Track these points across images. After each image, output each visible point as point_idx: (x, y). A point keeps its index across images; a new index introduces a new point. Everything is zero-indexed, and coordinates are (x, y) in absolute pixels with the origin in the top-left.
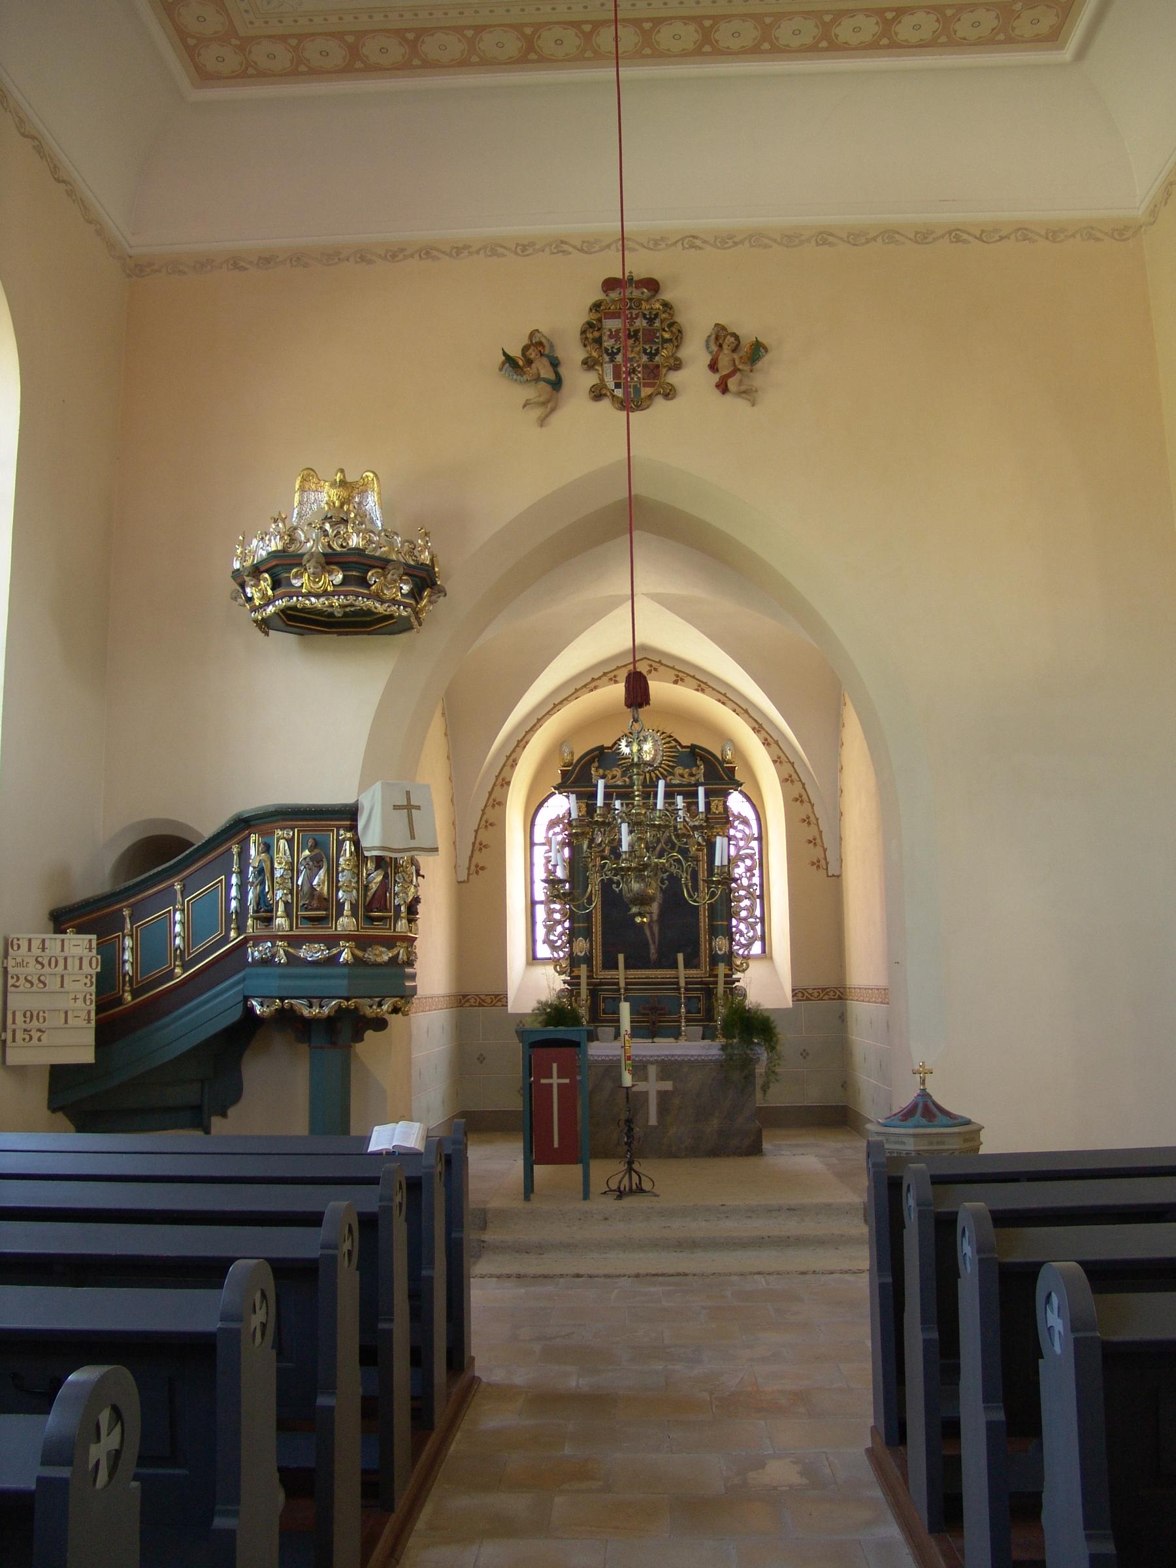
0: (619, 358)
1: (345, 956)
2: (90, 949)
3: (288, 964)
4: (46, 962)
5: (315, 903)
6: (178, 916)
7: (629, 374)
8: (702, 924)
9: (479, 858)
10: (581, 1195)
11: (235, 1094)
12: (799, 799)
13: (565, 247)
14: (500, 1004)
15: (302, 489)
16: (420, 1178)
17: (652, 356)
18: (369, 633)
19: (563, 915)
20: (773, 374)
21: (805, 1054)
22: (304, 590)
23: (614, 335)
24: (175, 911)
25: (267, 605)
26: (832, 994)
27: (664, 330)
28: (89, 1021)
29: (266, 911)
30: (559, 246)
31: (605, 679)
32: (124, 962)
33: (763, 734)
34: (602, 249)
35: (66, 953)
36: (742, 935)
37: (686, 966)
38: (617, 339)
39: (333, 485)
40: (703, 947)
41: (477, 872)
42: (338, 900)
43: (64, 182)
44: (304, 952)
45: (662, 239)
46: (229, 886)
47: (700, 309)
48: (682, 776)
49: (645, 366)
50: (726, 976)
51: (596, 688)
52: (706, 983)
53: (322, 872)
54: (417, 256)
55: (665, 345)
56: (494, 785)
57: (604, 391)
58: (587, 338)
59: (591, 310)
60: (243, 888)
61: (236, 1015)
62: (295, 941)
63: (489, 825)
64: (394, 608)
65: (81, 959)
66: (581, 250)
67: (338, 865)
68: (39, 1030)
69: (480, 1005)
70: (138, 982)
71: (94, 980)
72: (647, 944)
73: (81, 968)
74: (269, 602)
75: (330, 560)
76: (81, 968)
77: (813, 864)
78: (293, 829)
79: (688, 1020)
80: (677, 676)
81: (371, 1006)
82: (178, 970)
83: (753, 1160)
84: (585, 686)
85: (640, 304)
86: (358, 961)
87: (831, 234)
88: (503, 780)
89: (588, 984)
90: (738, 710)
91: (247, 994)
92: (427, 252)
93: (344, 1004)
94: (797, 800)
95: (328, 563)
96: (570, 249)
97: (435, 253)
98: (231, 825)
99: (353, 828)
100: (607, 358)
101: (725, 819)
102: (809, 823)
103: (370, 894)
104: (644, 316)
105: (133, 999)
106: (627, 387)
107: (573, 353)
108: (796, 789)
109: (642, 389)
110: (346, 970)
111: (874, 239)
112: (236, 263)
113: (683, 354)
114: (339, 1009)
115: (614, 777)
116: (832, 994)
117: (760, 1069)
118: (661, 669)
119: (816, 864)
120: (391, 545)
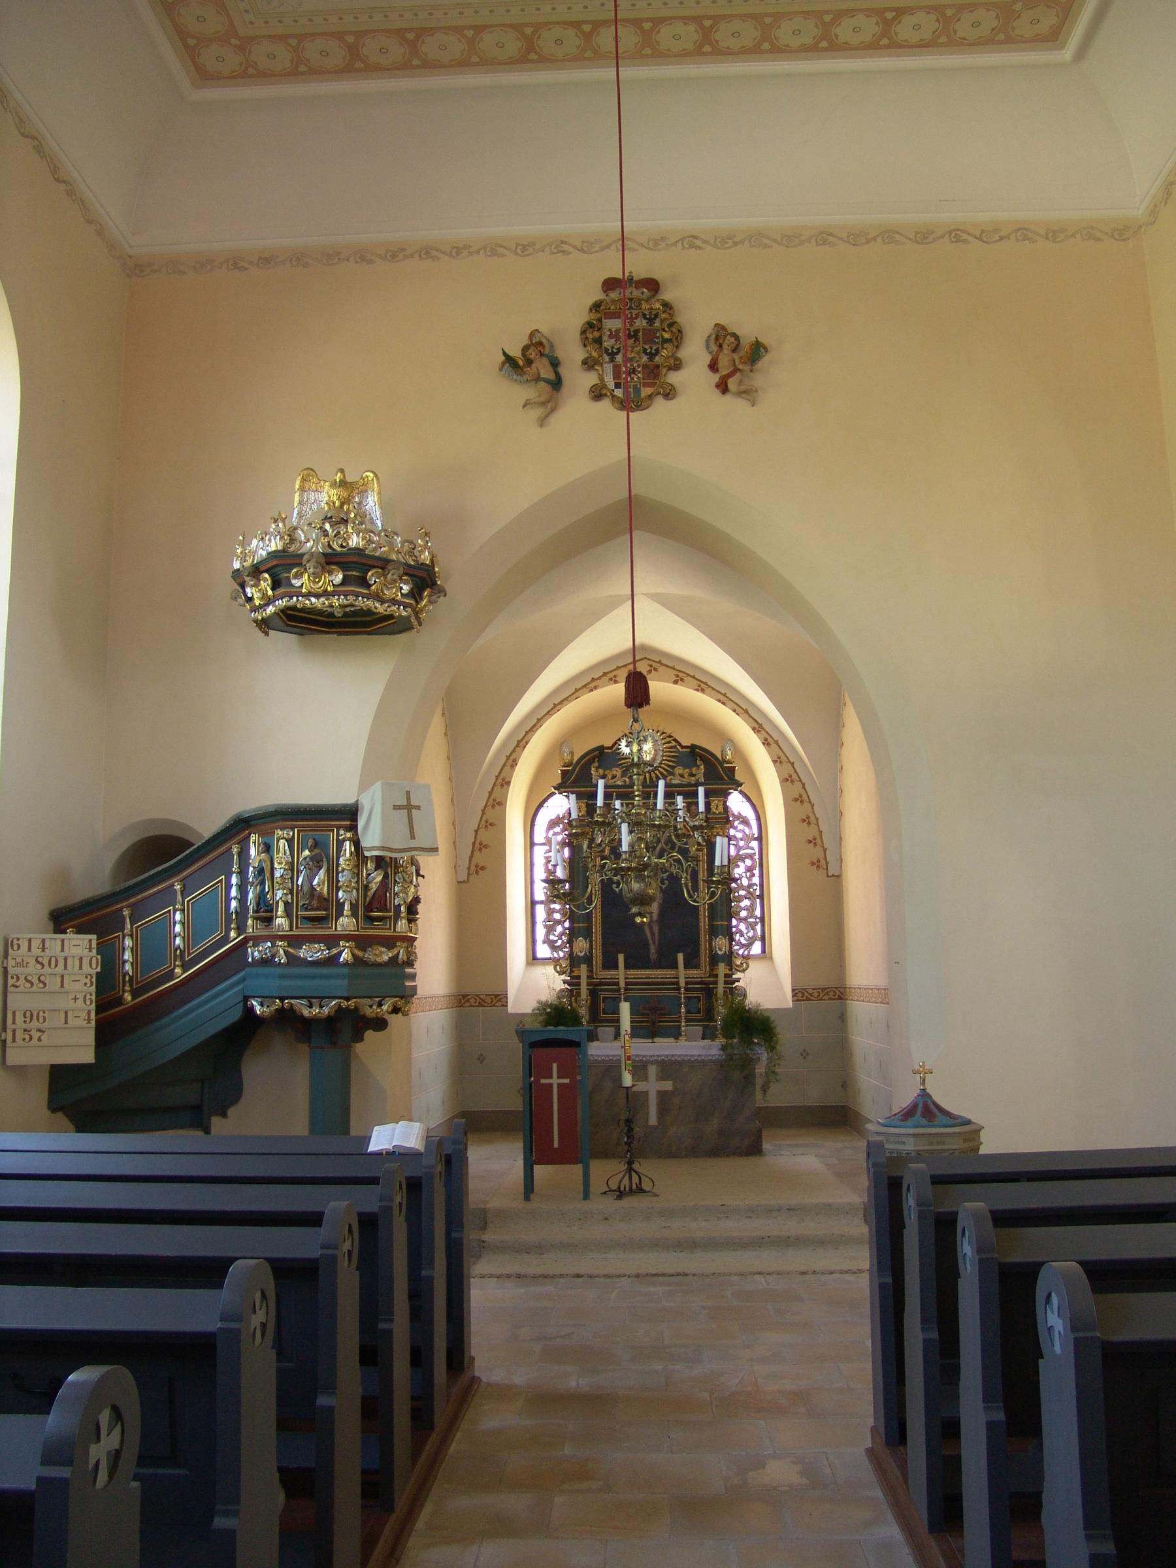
0: (619, 358)
1: (345, 956)
2: (90, 949)
3: (288, 964)
5: (315, 903)
6: (178, 916)
7: (629, 374)
8: (702, 924)
9: (479, 858)
10: (581, 1195)
11: (235, 1094)
12: (799, 799)
13: (565, 247)
14: (500, 1004)
15: (302, 489)
17: (652, 356)
18: (369, 633)
19: (563, 915)
20: (773, 374)
21: (805, 1054)
22: (304, 590)
23: (614, 335)
24: (175, 911)
25: (267, 605)
26: (832, 994)
27: (664, 330)
28: (89, 1021)
29: (266, 911)
30: (559, 246)
31: (605, 679)
32: (124, 962)
33: (763, 734)
34: (602, 249)
35: (66, 953)
36: (742, 935)
37: (686, 966)
38: (617, 339)
39: (333, 485)
40: (703, 947)
41: (477, 872)
42: (338, 900)
43: (64, 182)
44: (304, 952)
45: (662, 239)
46: (229, 886)
47: (700, 309)
48: (682, 776)
49: (645, 366)
50: (726, 976)
51: (596, 688)
52: (706, 983)
53: (322, 872)
54: (417, 256)
55: (665, 345)
56: (494, 785)
57: (604, 391)
58: (587, 338)
59: (591, 310)
60: (243, 888)
61: (236, 1015)
62: (295, 941)
63: (489, 825)
64: (394, 608)
65: (81, 959)
66: (581, 250)
67: (338, 865)
68: (39, 1030)
69: (480, 1005)
70: (138, 982)
71: (94, 980)
72: (647, 944)
73: (81, 968)
74: (269, 602)
75: (330, 560)
76: (81, 968)
77: (813, 864)
78: (293, 829)
79: (688, 1020)
80: (677, 676)
81: (371, 1006)
82: (178, 970)
83: (753, 1160)
84: (585, 686)
85: (640, 304)
86: (358, 961)
87: (831, 234)
88: (503, 780)
89: (588, 984)
90: (738, 710)
91: (247, 994)
92: (427, 252)
93: (344, 1004)
94: (797, 800)
95: (328, 563)
96: (570, 249)
97: (435, 253)
98: (231, 825)
99: (353, 828)
100: (607, 358)
101: (725, 819)
102: (809, 823)
103: (370, 894)
104: (644, 316)
105: (133, 999)
106: (627, 387)
107: (573, 353)
108: (796, 789)
109: (642, 389)
110: (346, 970)
111: (874, 239)
112: (236, 263)
113: (683, 354)
114: (339, 1009)
115: (614, 777)
116: (832, 994)
117: (760, 1069)
118: (661, 669)
119: (816, 864)
120: (391, 545)
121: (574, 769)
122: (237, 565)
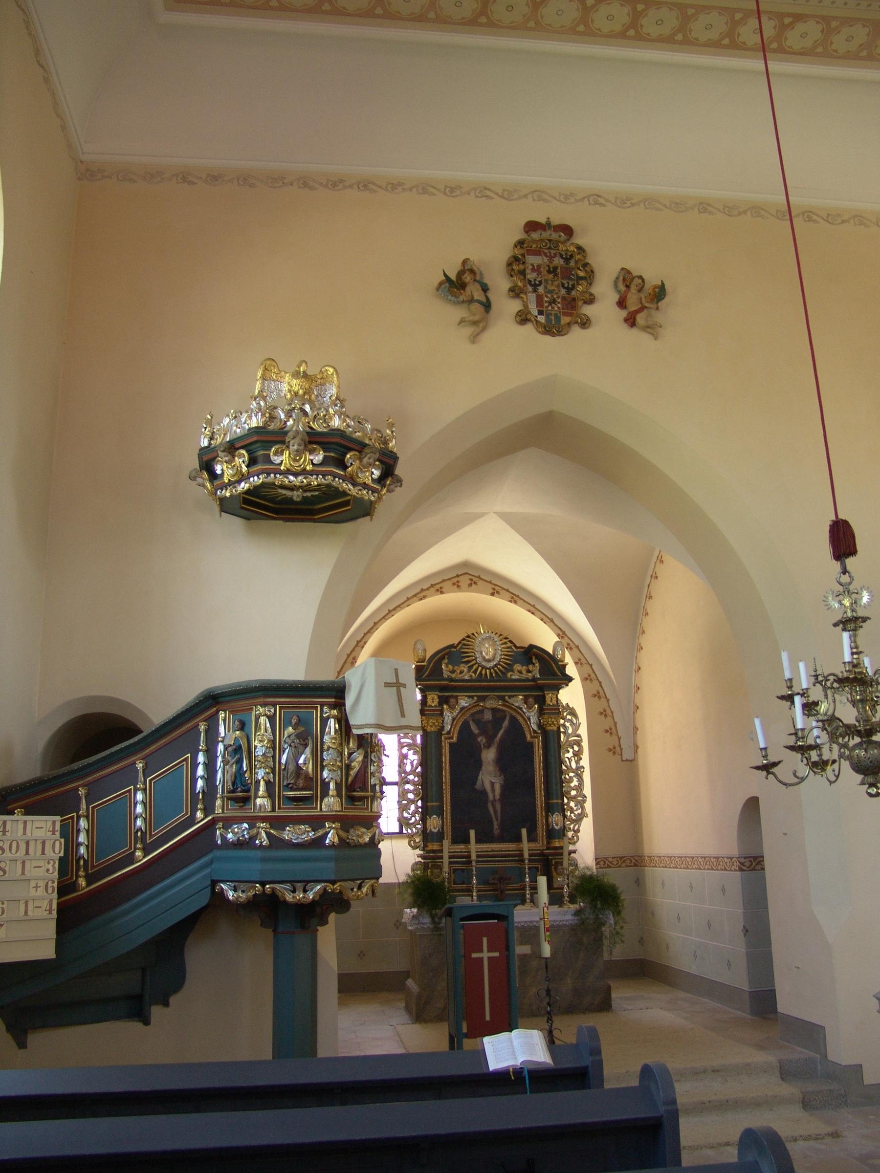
0: (541, 289)
1: (331, 838)
2: (54, 832)
3: (270, 847)
4: (6, 847)
5: (301, 783)
6: (140, 796)
7: (550, 303)
11: (177, 982)
12: (597, 695)
13: (488, 193)
15: (264, 378)
16: (660, 1118)
17: (569, 290)
18: (315, 521)
20: (671, 312)
22: (282, 468)
23: (537, 269)
24: (136, 790)
25: (239, 482)
26: (628, 861)
27: (579, 269)
29: (242, 791)
30: (483, 191)
31: (433, 590)
32: (79, 844)
34: (520, 198)
38: (539, 273)
39: (296, 375)
42: (323, 780)
43: (42, 67)
44: (289, 834)
45: (572, 194)
46: (195, 766)
47: (609, 252)
48: (520, 672)
49: (564, 299)
51: (425, 597)
53: (308, 750)
54: (355, 187)
55: (580, 282)
57: (529, 317)
58: (513, 270)
59: (516, 246)
60: (210, 767)
61: (203, 899)
62: (278, 822)
64: (365, 492)
65: (44, 843)
66: (502, 197)
67: (322, 743)
70: (93, 867)
71: (57, 865)
73: (43, 853)
74: (243, 478)
75: (313, 439)
76: (43, 853)
77: (610, 750)
78: (274, 705)
80: (494, 589)
82: (139, 854)
84: (415, 595)
85: (558, 245)
86: (343, 843)
87: (709, 205)
90: (545, 619)
91: (215, 878)
92: (365, 185)
93: (330, 888)
95: (310, 443)
96: (491, 194)
97: (371, 186)
98: (201, 701)
99: (340, 705)
100: (530, 289)
101: (557, 710)
103: (352, 773)
104: (561, 256)
105: (88, 885)
106: (548, 316)
107: (500, 283)
108: (595, 687)
109: (562, 317)
110: (332, 852)
111: (745, 212)
112: (185, 177)
113: (594, 290)
114: (324, 893)
115: (461, 672)
116: (628, 861)
117: (606, 930)
118: (480, 583)
119: (612, 750)
120: (363, 430)
121: (428, 666)
122: (205, 443)
